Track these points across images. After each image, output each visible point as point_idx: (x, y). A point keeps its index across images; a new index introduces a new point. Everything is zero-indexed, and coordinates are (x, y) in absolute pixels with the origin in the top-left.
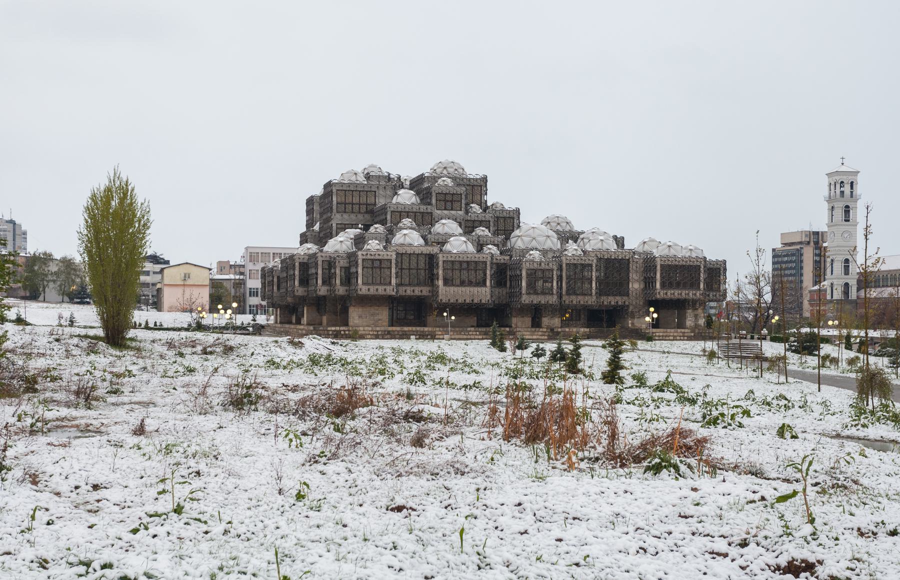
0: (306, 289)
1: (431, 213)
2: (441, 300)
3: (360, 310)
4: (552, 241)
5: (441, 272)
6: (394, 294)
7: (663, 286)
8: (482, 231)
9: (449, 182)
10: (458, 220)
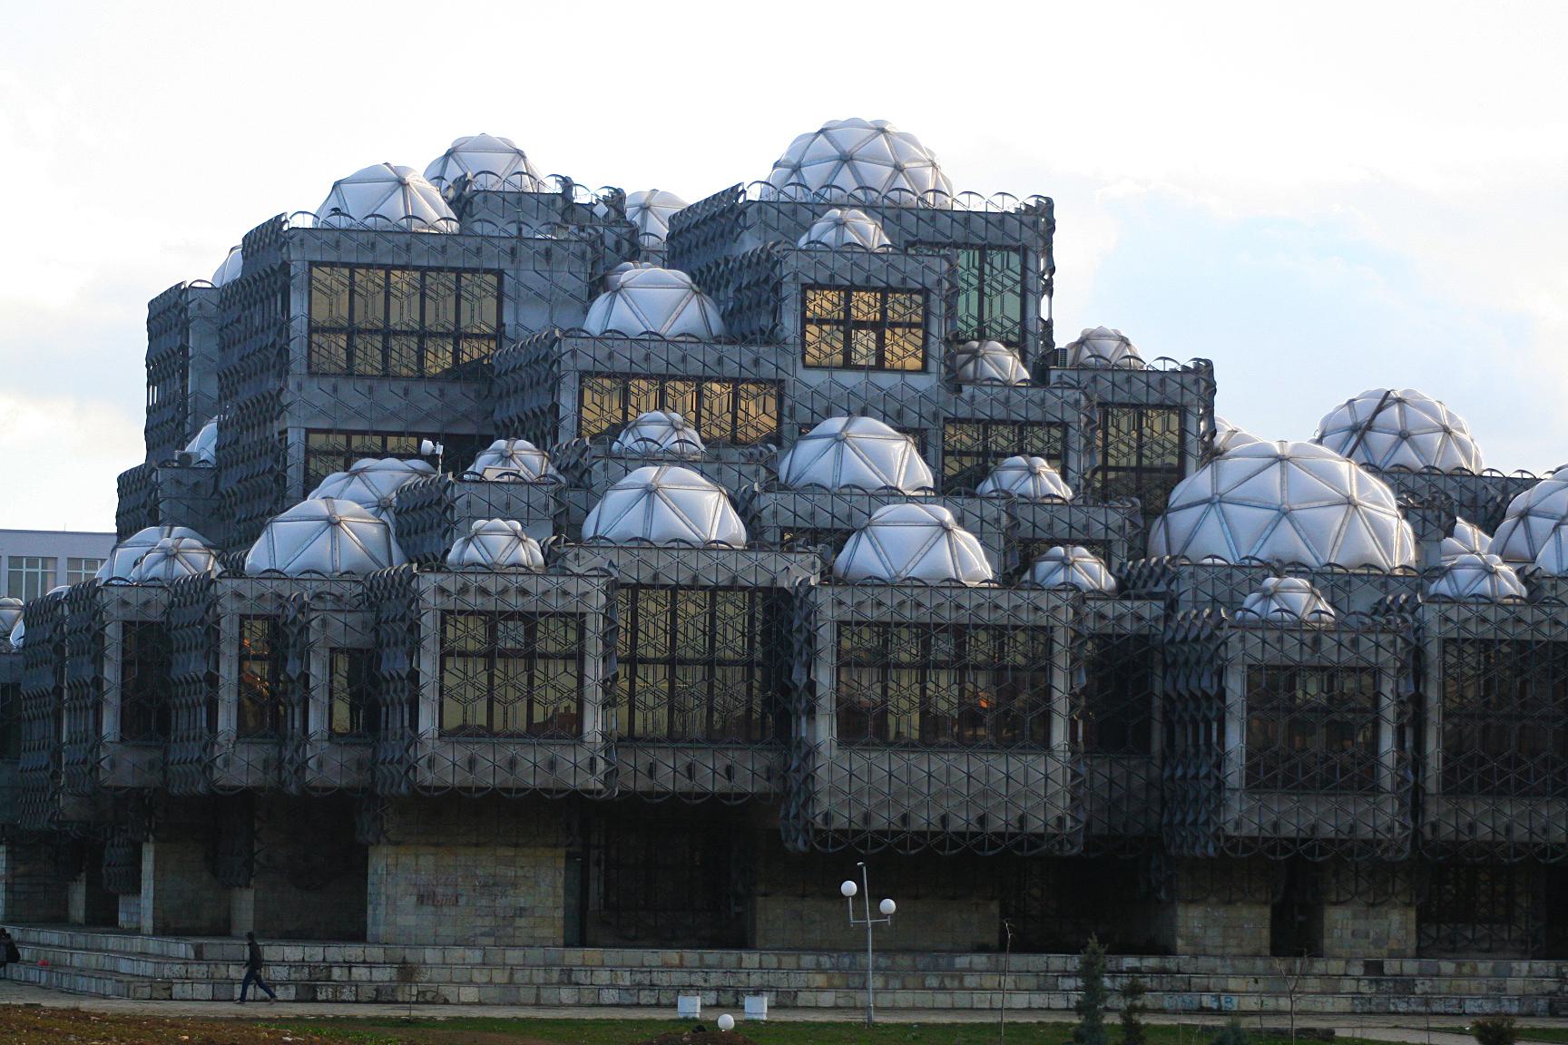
1: (779, 383)
2: (827, 817)
3: (427, 861)
6: (594, 783)
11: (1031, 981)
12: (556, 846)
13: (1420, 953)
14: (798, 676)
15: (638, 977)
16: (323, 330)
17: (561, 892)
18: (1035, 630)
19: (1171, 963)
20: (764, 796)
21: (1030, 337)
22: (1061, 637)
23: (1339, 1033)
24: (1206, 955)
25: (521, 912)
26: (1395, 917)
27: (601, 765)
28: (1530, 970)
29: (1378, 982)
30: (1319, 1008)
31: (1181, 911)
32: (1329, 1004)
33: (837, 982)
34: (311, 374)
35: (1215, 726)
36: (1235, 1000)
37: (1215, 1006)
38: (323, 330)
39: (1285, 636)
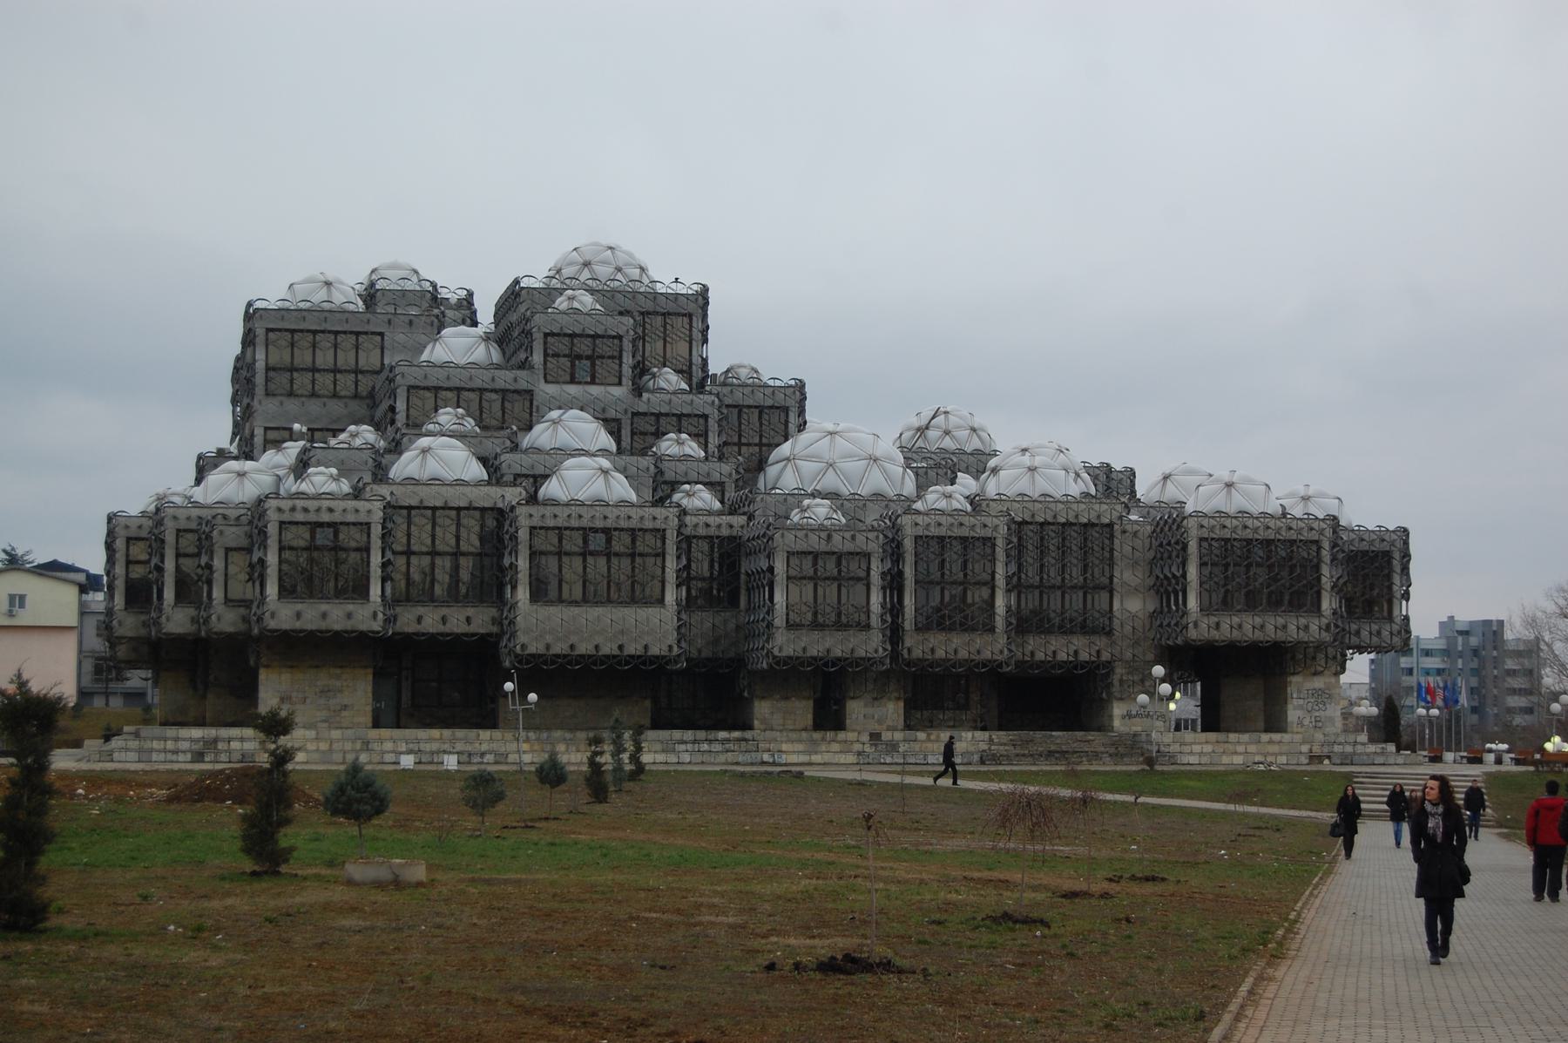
0: (143, 617)
1: (530, 393)
2: (523, 646)
3: (286, 677)
4: (884, 471)
5: (523, 563)
6: (376, 626)
7: (286, 591)
8: (676, 446)
9: (586, 301)
10: (611, 414)
11: (658, 747)
12: (366, 667)
13: (908, 727)
14: (506, 562)
15: (411, 746)
16: (274, 369)
17: (370, 695)
18: (985, 540)
19: (748, 734)
20: (490, 635)
21: (694, 367)
22: (1326, 545)
23: (806, 773)
24: (772, 730)
25: (345, 707)
26: (891, 706)
27: (380, 616)
28: (973, 737)
29: (876, 745)
30: (836, 761)
31: (756, 703)
32: (843, 759)
33: (536, 747)
34: (267, 394)
35: (1180, 594)
36: (784, 756)
37: (771, 760)
38: (274, 369)
39: (810, 534)
